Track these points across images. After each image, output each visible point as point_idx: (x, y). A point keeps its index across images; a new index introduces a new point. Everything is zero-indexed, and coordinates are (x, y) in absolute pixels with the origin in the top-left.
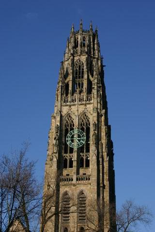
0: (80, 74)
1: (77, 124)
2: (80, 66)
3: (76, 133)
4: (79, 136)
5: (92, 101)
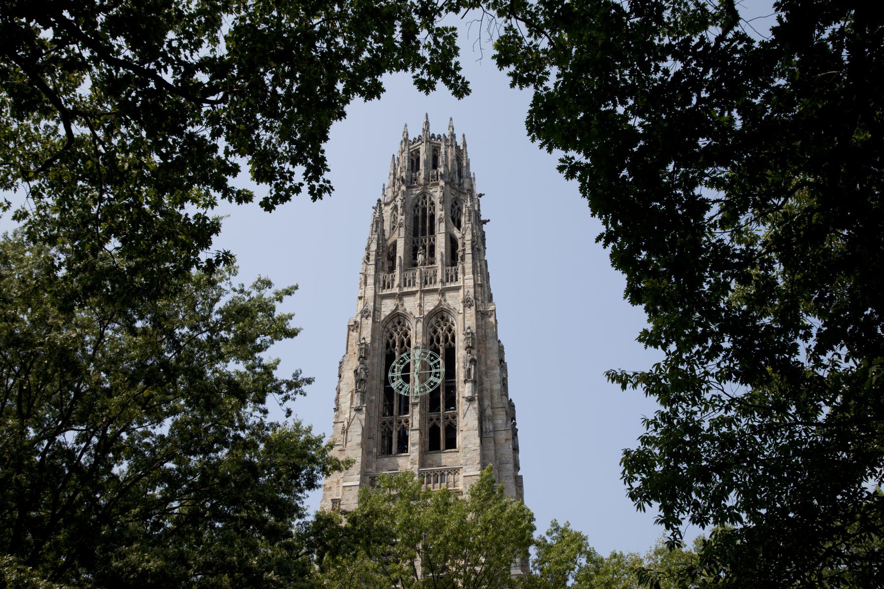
0: (424, 223)
5: (460, 283)
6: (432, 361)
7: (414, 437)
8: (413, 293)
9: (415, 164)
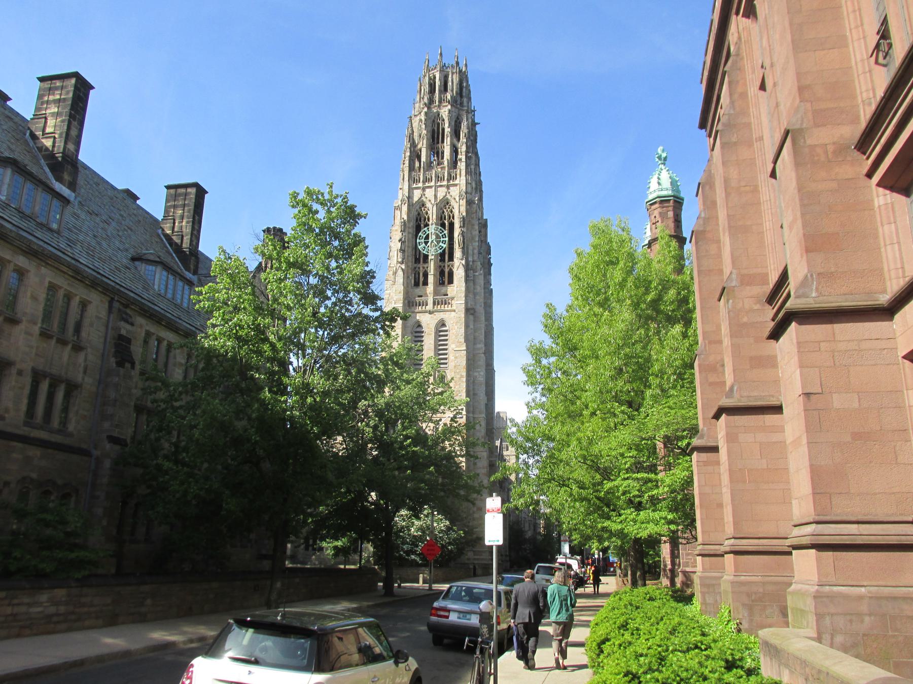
4: (437, 236)
5: (457, 182)
7: (431, 279)
8: (430, 187)
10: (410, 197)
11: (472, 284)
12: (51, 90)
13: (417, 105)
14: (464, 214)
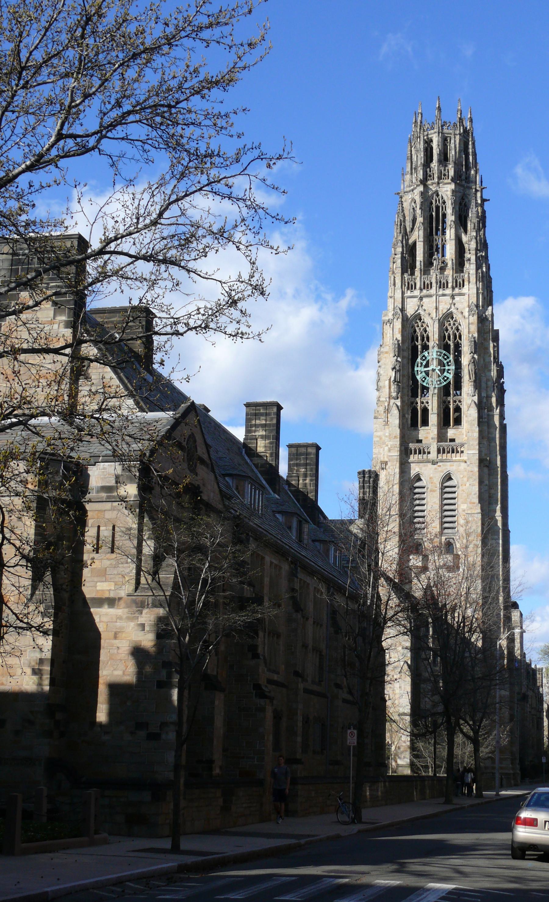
1: (436, 336)
2: (437, 208)
3: (435, 356)
4: (441, 363)
5: (465, 290)
6: (446, 359)
8: (430, 296)
9: (429, 153)
10: (403, 310)
11: (485, 428)
12: (257, 415)
13: (408, 177)
14: (476, 335)
